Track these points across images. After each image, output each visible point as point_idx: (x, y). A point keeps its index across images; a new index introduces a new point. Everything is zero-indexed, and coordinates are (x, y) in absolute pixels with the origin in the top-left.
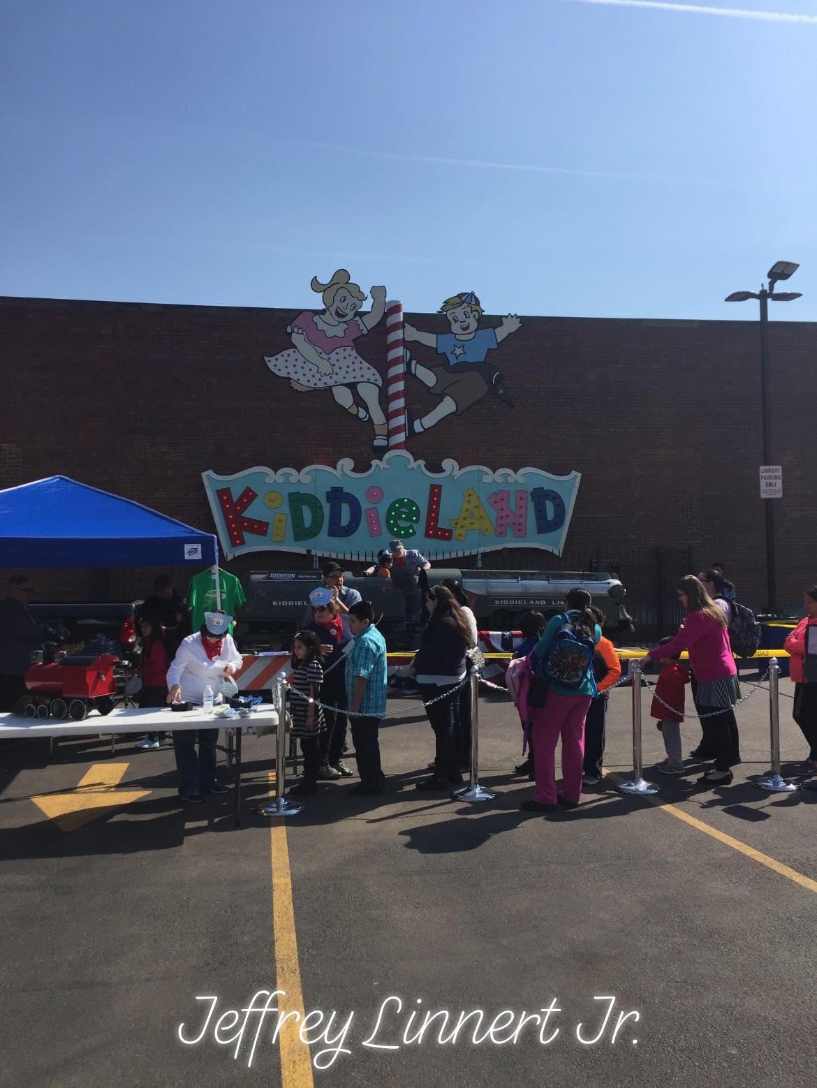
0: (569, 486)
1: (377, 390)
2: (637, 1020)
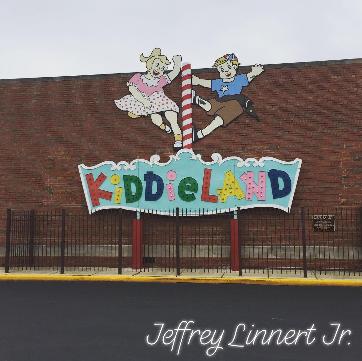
0: (294, 168)
1: (176, 115)
2: (350, 334)
